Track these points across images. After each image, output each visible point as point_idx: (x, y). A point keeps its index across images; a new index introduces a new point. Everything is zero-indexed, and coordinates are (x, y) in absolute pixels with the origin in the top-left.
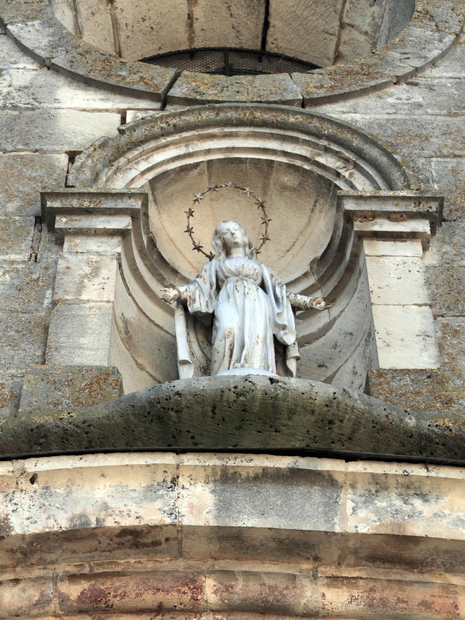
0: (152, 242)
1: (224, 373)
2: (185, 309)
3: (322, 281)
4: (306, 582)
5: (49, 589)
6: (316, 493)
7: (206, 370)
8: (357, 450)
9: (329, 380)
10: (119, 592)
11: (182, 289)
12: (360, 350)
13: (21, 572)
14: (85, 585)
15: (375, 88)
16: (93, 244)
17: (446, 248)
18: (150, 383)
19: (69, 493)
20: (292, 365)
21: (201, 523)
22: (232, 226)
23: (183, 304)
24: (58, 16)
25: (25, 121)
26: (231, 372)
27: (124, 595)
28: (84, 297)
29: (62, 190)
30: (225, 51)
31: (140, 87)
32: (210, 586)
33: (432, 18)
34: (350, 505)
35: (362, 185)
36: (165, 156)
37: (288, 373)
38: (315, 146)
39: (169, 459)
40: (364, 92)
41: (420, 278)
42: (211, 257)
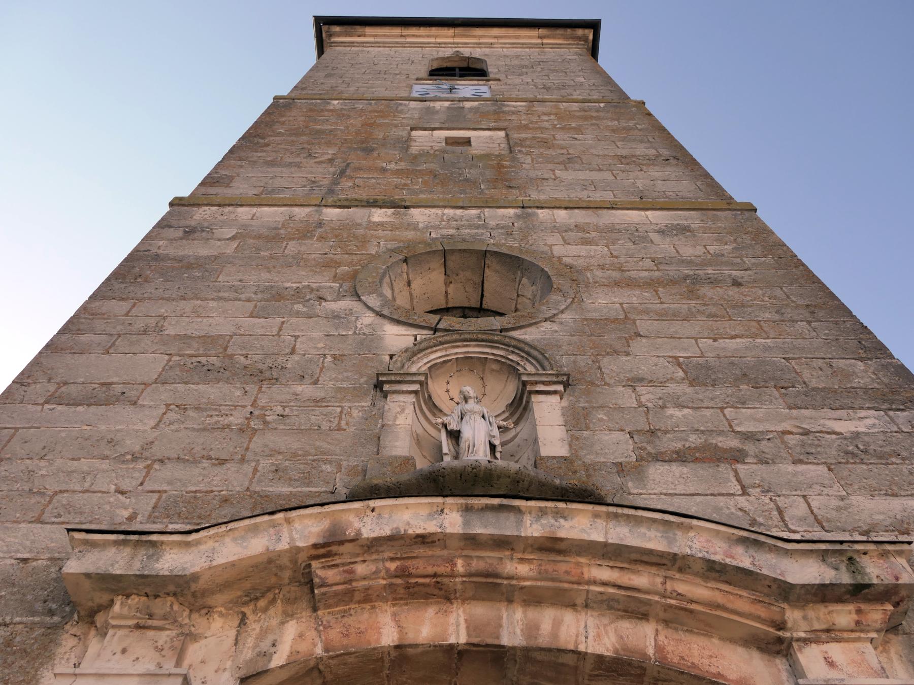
0: (430, 397)
1: (465, 458)
2: (446, 428)
3: (512, 415)
4: (508, 561)
5: (380, 565)
6: (512, 517)
7: (456, 457)
8: (532, 495)
9: (517, 462)
10: (874, 377)
11: (445, 418)
12: (531, 447)
13: (366, 557)
14: (398, 563)
15: (535, 323)
16: (401, 398)
17: (571, 398)
18: (430, 464)
19: (391, 517)
20: (498, 455)
21: (456, 532)
22: (468, 388)
23: (445, 426)
24: (384, 292)
25: (369, 341)
26: (469, 458)
27: (417, 568)
28: (397, 422)
29: (387, 372)
30: (463, 308)
31: (424, 324)
32: (460, 563)
33: (561, 291)
34: (529, 522)
35: (530, 369)
36: (435, 356)
37: (496, 458)
38: (507, 350)
39: (440, 500)
40: (530, 325)
41: (559, 412)
42: (458, 404)
